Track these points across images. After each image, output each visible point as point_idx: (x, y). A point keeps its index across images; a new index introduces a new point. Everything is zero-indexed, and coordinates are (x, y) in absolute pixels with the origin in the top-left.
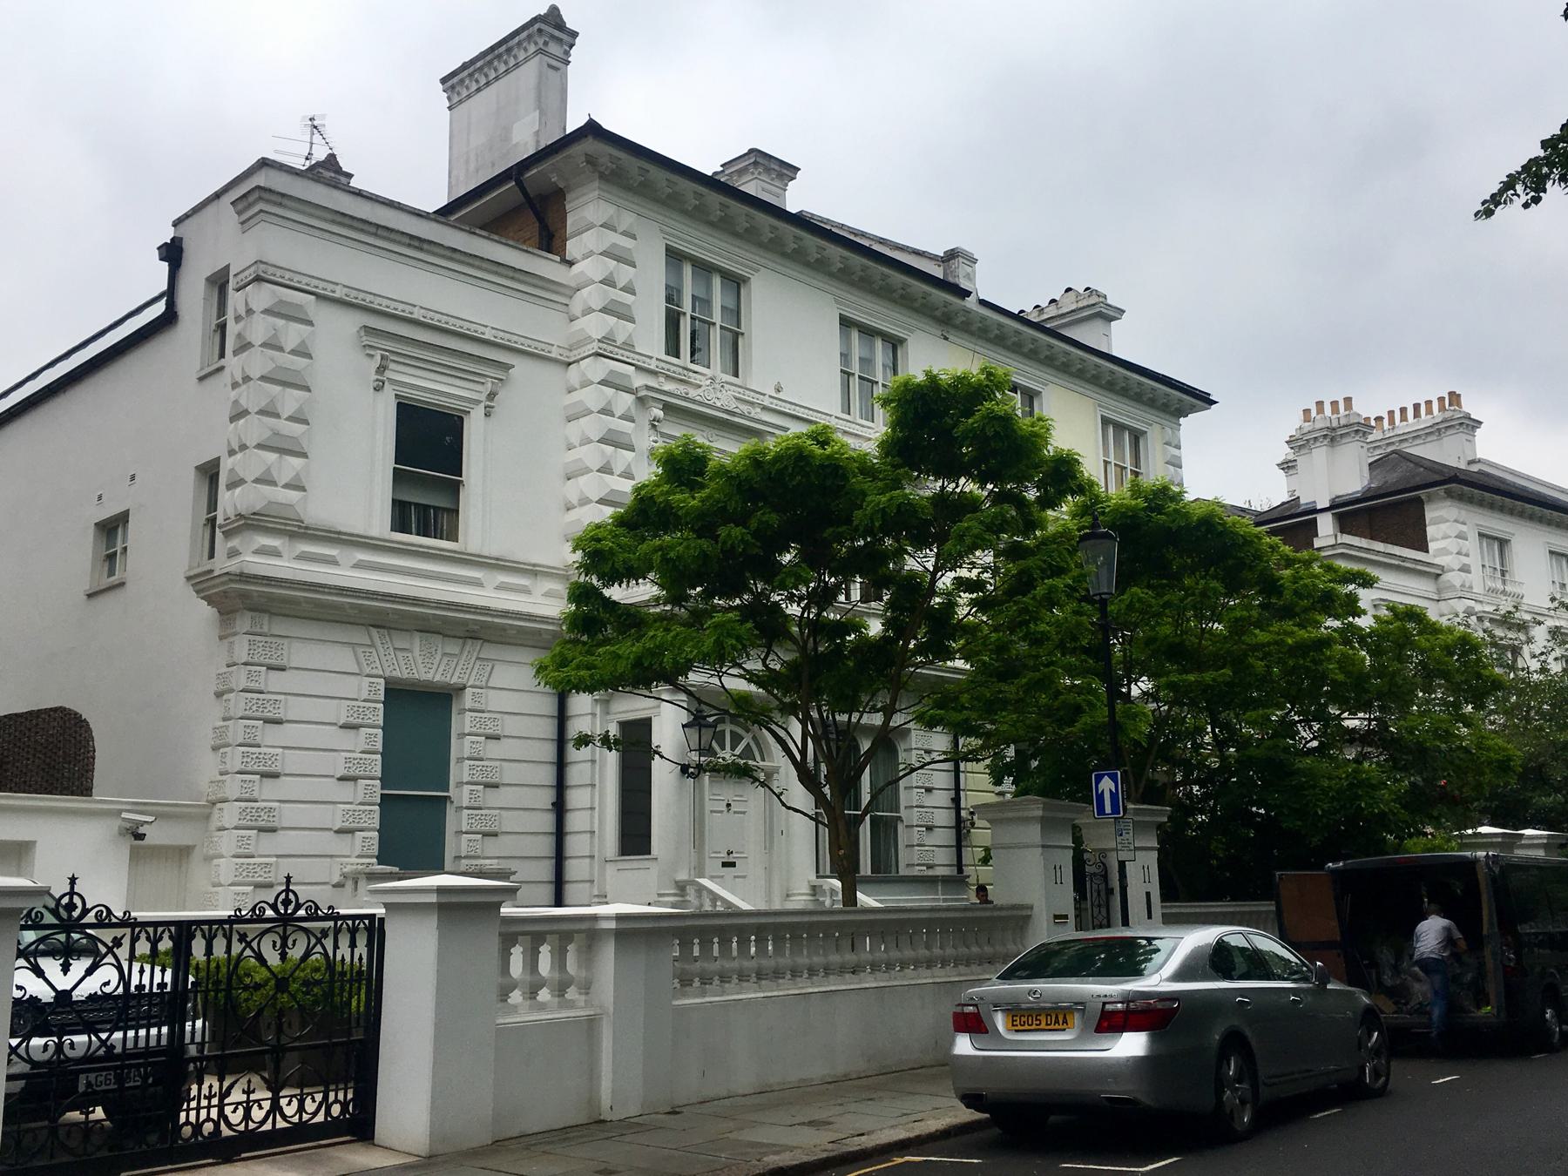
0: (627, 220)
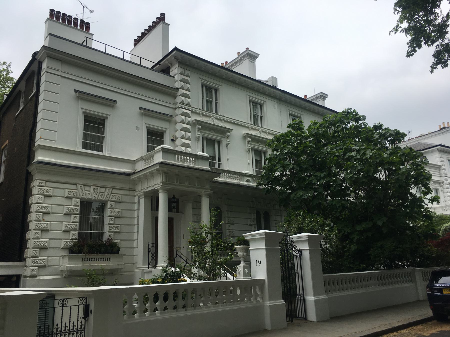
0: (187, 72)
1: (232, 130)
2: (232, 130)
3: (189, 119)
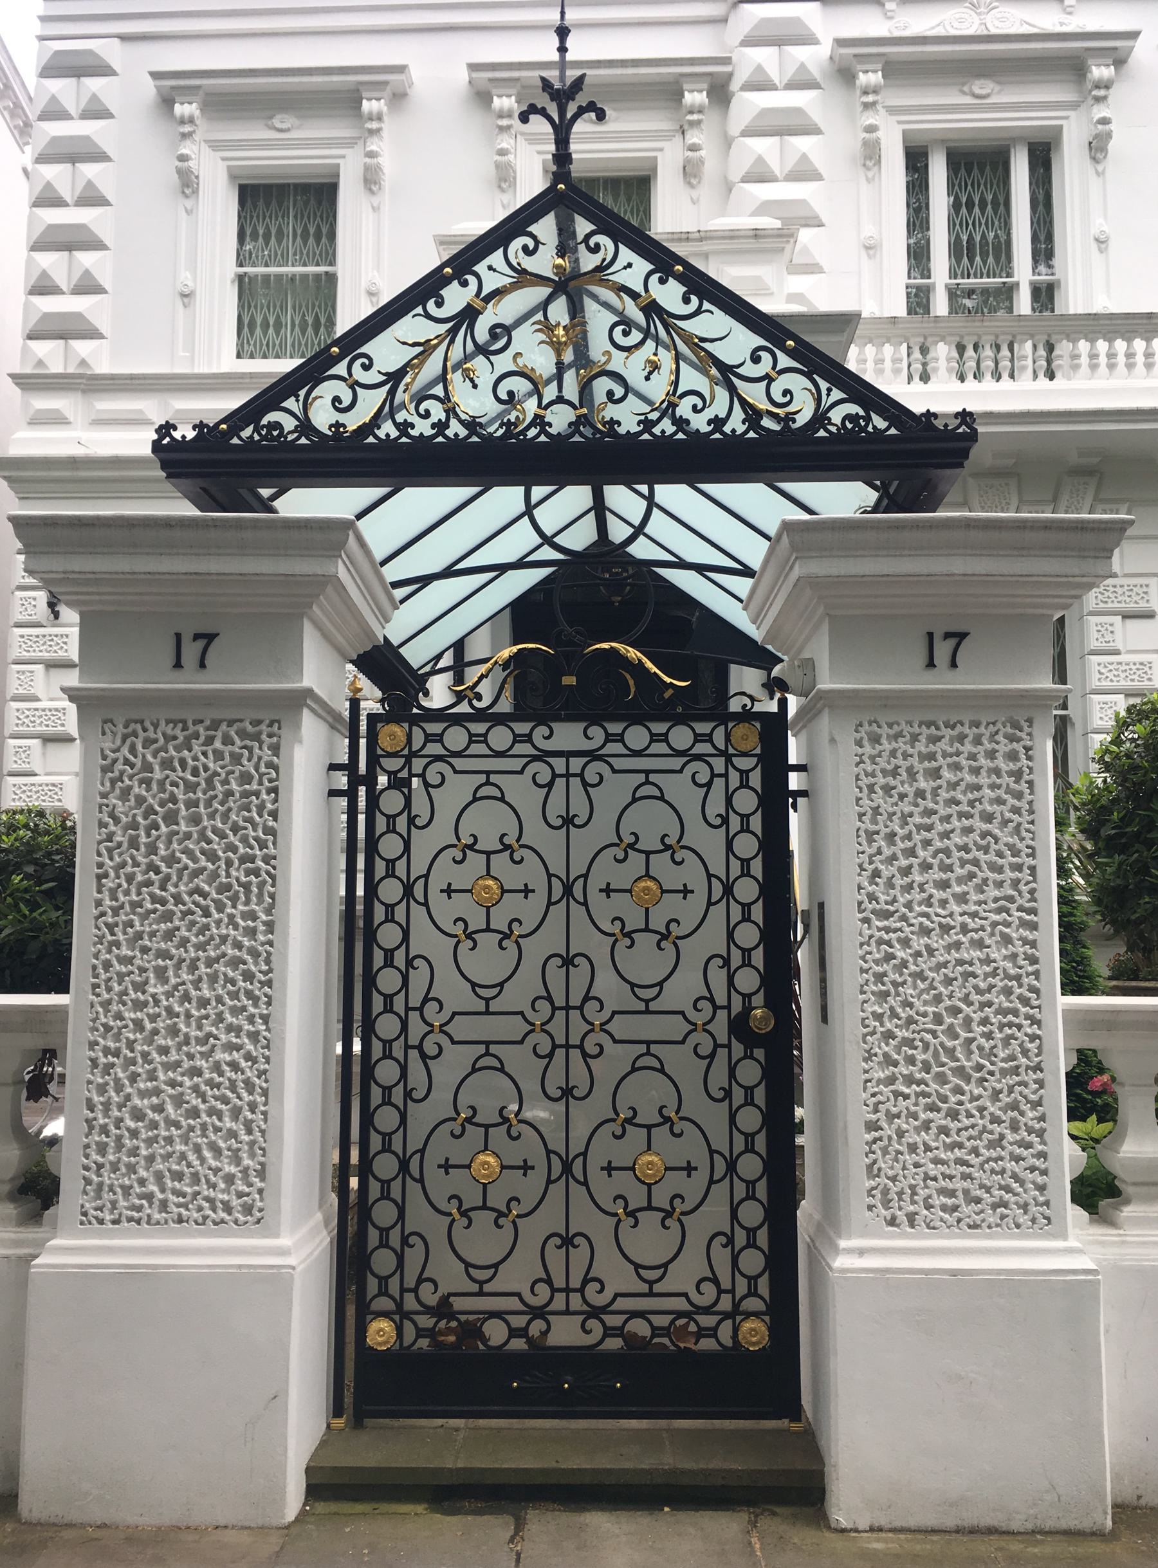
1: (1134, 35)
2: (1134, 35)
3: (800, 54)
